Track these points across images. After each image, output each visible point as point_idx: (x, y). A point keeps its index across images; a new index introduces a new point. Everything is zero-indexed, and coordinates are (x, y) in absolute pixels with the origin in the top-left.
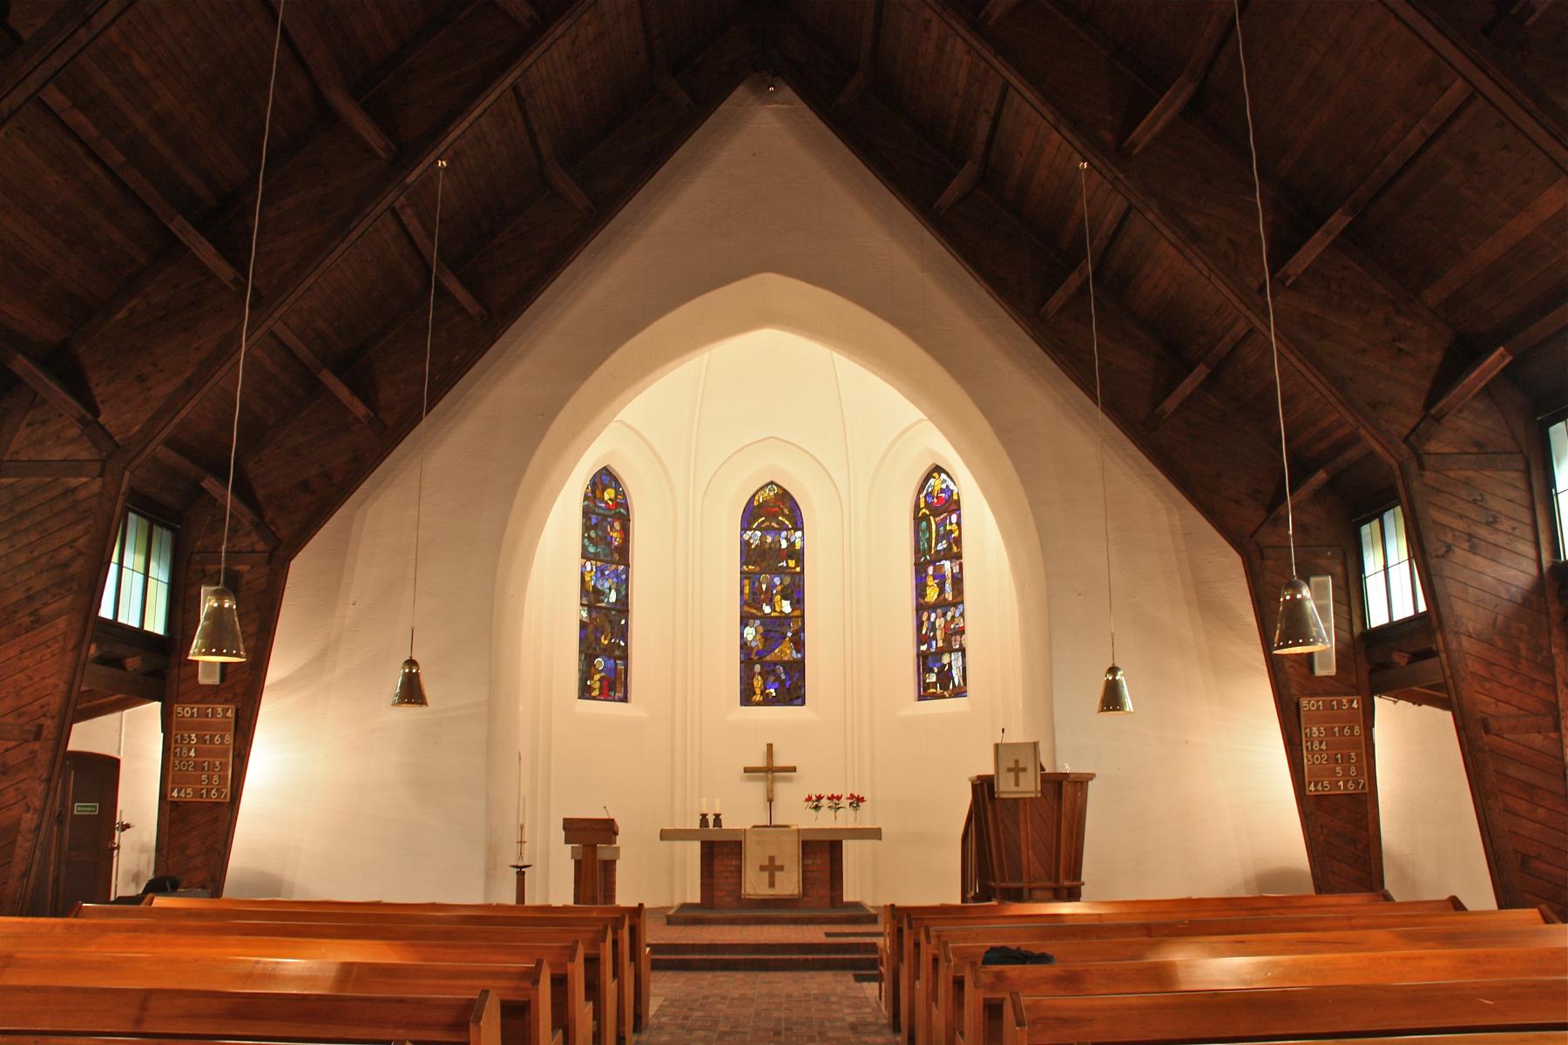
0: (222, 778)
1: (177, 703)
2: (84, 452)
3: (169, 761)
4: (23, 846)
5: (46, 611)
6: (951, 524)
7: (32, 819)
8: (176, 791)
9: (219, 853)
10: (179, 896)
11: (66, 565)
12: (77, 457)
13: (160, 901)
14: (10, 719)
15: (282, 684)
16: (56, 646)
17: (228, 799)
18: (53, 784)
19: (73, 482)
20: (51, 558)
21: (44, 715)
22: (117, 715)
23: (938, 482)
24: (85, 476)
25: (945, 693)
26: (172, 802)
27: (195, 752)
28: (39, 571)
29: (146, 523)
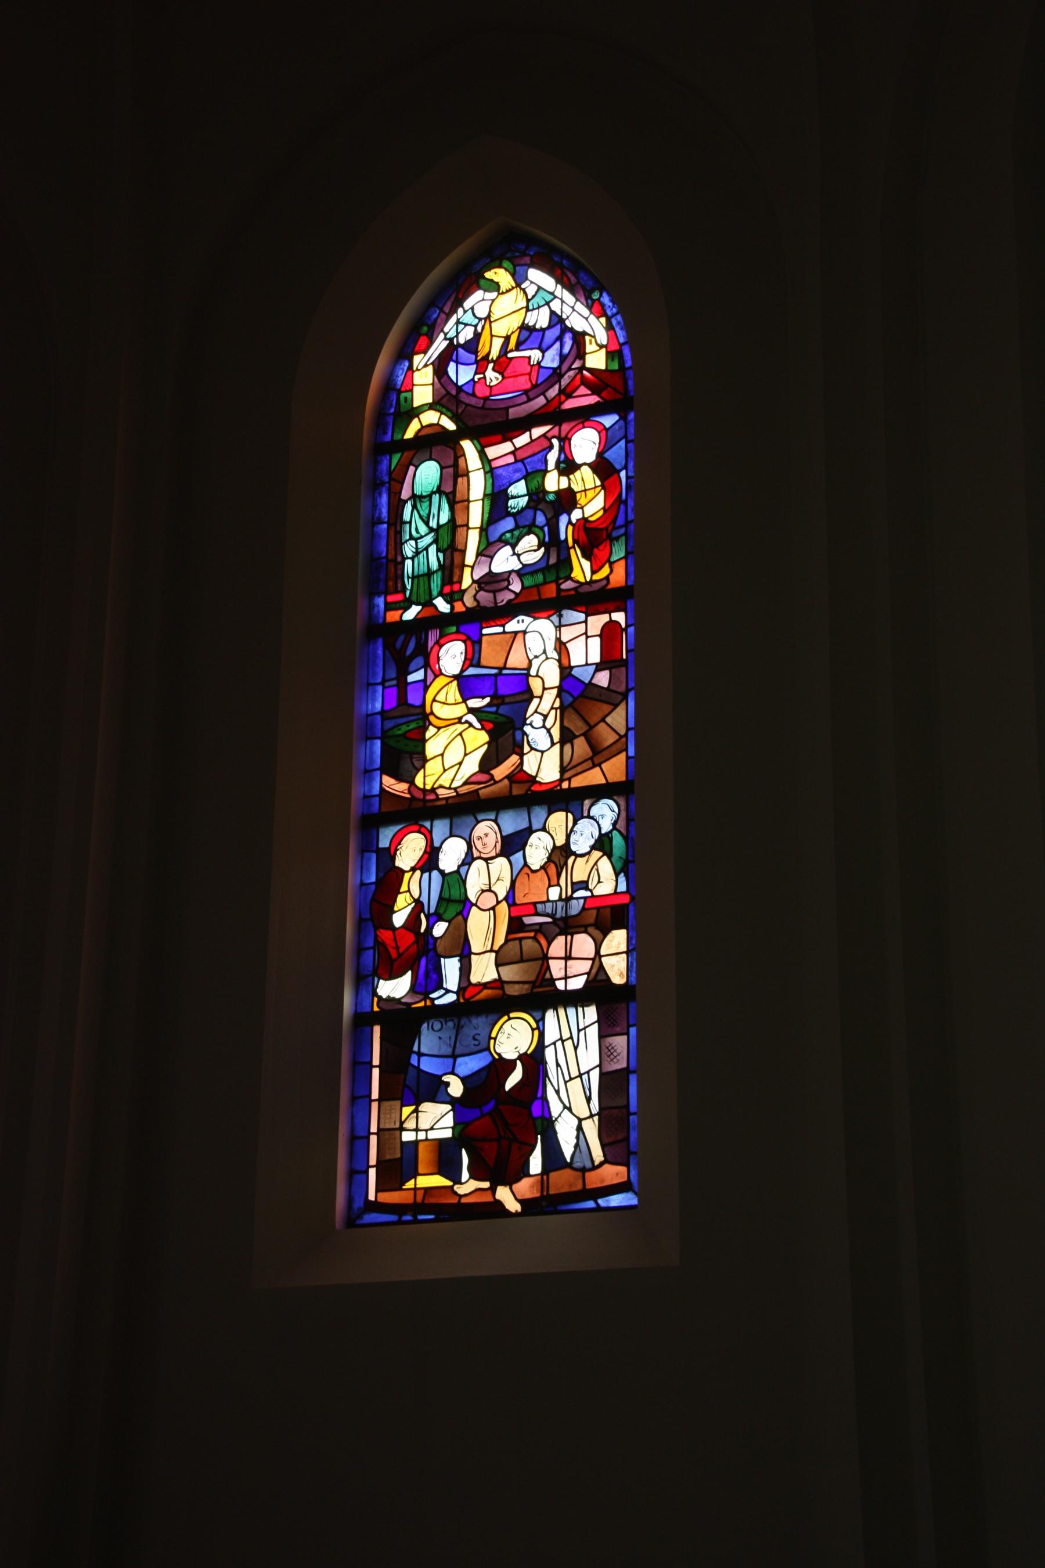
6: (568, 466)
23: (512, 301)
25: (503, 1194)
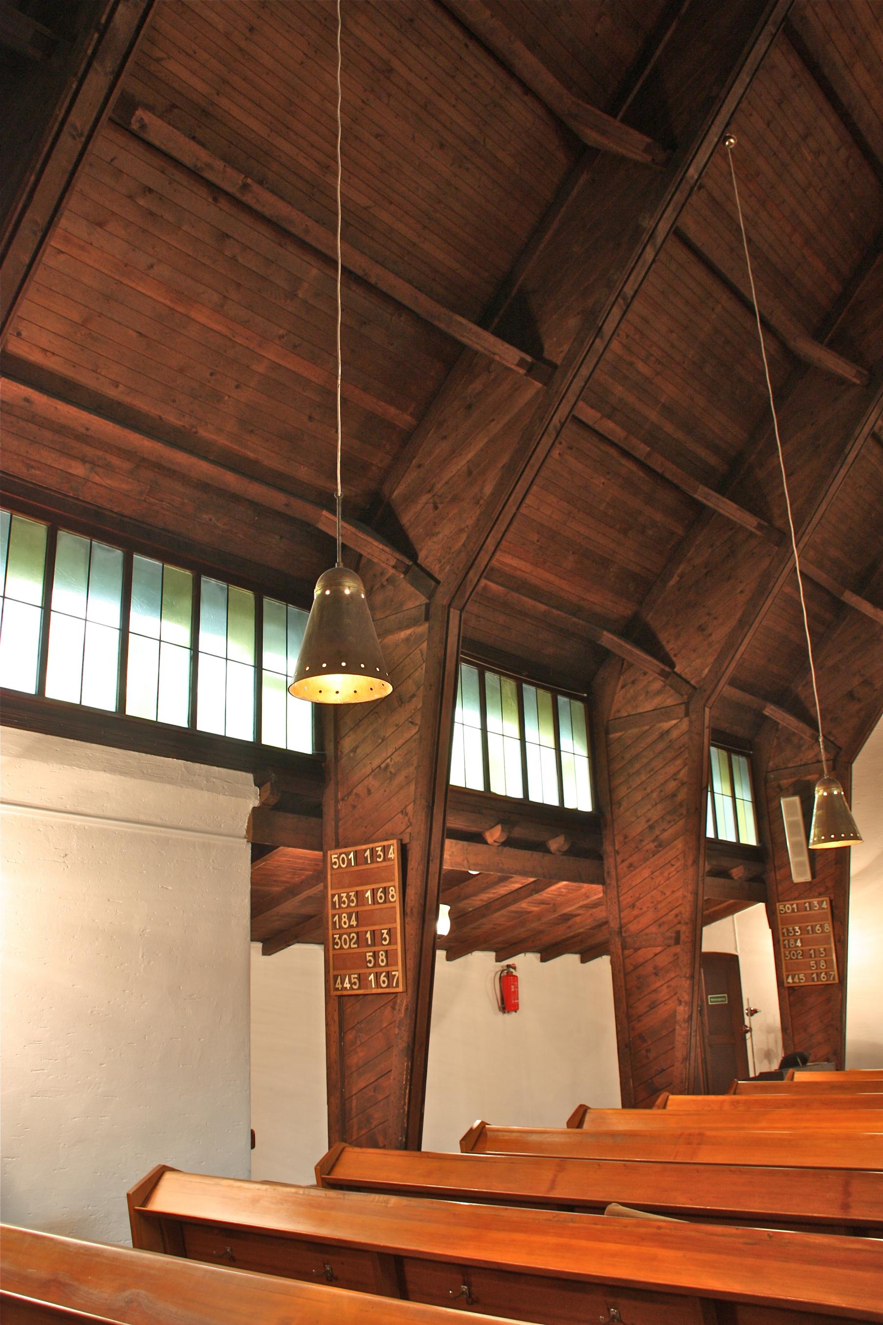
0: (828, 963)
1: (779, 901)
2: (670, 699)
3: (780, 953)
4: (681, 1033)
5: (665, 836)
7: (685, 1010)
8: (790, 978)
9: (837, 1029)
10: (810, 1070)
11: (674, 795)
12: (665, 705)
13: (801, 1076)
14: (653, 929)
15: (864, 872)
16: (679, 864)
17: (837, 981)
18: (696, 981)
19: (666, 725)
20: (661, 791)
21: (679, 923)
22: (729, 918)
24: (674, 719)
26: (789, 988)
27: (801, 942)
28: (654, 804)
29: (725, 753)
